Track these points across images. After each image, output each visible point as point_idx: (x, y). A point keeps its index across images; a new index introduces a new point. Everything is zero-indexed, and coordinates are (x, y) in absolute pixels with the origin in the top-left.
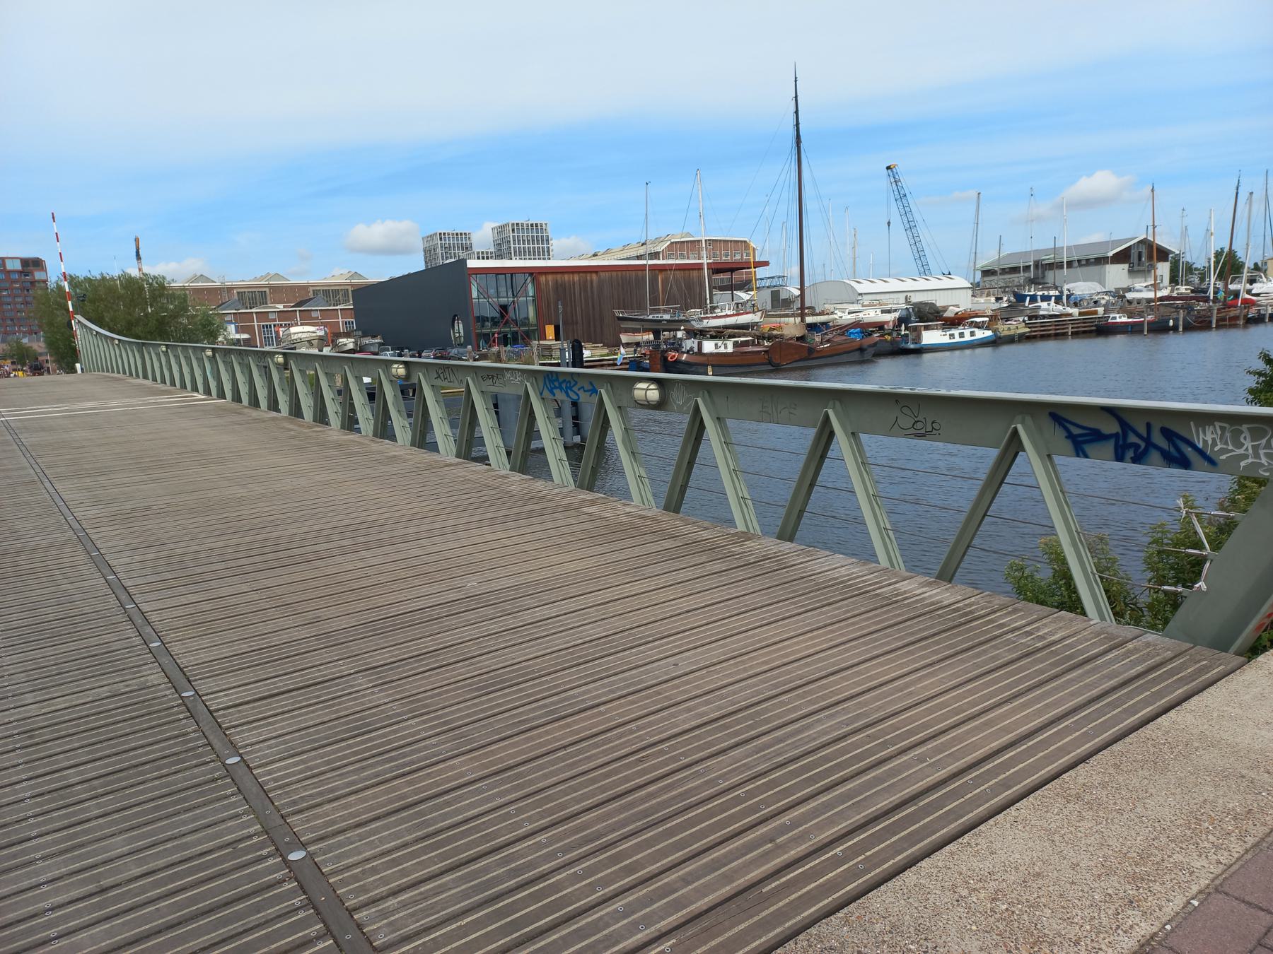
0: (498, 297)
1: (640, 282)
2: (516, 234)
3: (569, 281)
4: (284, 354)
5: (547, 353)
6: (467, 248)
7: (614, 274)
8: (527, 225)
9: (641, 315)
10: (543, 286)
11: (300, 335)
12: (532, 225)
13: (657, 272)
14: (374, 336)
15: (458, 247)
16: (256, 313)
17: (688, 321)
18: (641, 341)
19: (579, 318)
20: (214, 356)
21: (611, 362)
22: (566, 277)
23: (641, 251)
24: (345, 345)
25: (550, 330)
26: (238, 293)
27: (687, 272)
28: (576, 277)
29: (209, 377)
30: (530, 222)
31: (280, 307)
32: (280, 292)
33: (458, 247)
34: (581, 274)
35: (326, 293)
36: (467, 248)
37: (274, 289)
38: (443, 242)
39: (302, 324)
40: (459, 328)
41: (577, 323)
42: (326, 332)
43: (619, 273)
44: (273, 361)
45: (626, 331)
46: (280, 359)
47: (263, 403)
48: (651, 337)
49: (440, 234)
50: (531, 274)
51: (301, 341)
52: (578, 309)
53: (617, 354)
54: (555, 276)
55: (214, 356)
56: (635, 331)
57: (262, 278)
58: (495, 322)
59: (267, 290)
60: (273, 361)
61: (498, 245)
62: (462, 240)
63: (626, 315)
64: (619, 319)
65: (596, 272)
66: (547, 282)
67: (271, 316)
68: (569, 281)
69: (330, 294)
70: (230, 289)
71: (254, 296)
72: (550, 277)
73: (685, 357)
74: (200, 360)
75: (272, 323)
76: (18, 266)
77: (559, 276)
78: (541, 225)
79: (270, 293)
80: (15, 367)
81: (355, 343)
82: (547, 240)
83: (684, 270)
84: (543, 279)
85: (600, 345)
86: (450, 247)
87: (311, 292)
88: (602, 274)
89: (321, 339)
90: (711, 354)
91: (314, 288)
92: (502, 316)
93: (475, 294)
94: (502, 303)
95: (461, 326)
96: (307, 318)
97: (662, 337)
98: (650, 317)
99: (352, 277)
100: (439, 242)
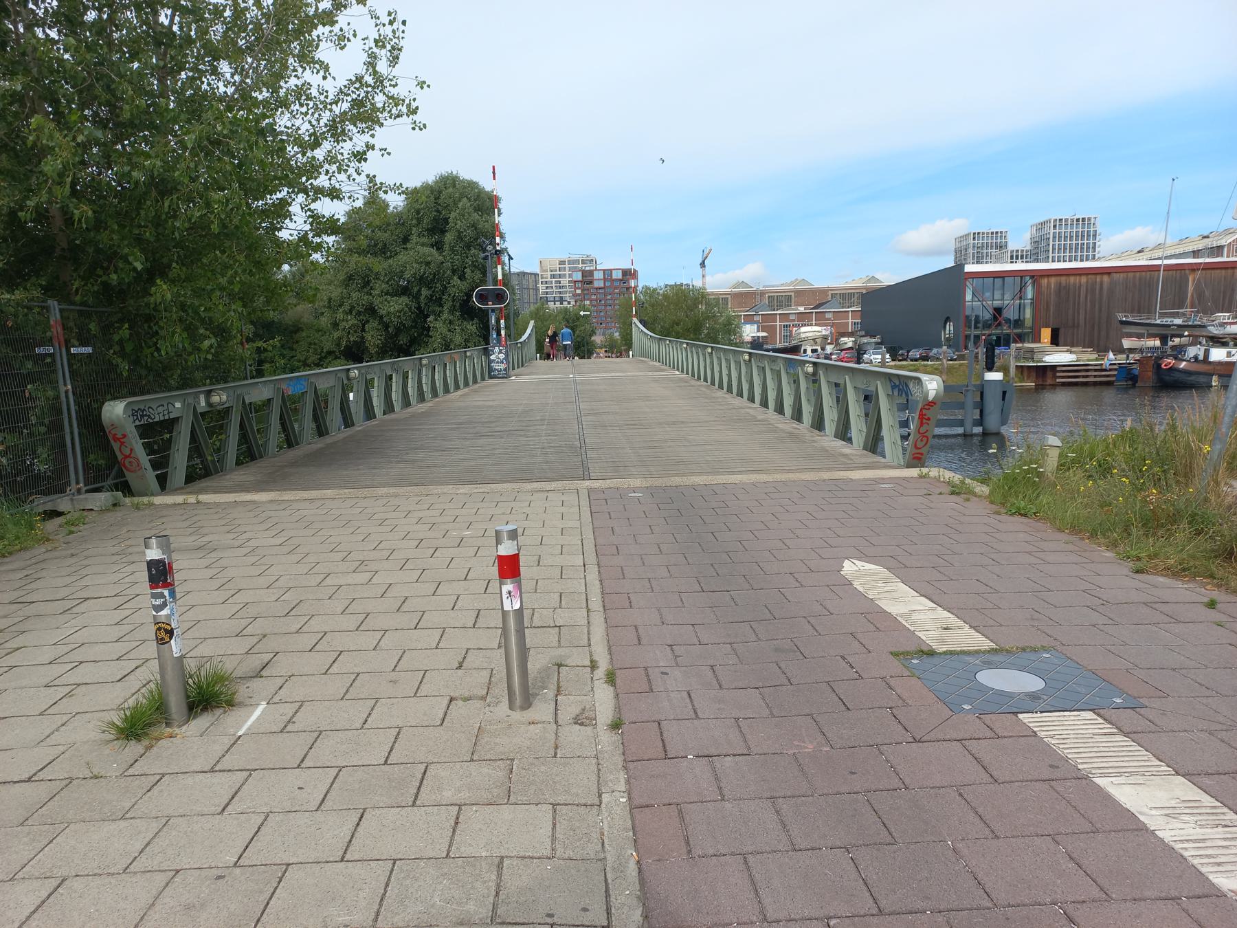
0: (993, 300)
1: (1150, 286)
2: (1057, 231)
3: (1075, 284)
4: (815, 364)
5: (1029, 355)
6: (1001, 247)
7: (1131, 275)
8: (1072, 220)
9: (1149, 319)
10: (1044, 289)
11: (807, 334)
12: (992, 233)
13: (1187, 272)
14: (872, 336)
15: (992, 247)
16: (780, 314)
17: (1204, 327)
18: (1144, 347)
19: (1082, 322)
20: (750, 360)
21: (1099, 368)
22: (1072, 279)
23: (1200, 245)
24: (846, 343)
25: (1046, 334)
26: (769, 297)
27: (1230, 271)
28: (1084, 279)
29: (743, 377)
30: (1075, 217)
31: (801, 309)
32: (803, 295)
33: (992, 247)
34: (1090, 276)
35: (843, 296)
36: (1001, 247)
37: (799, 293)
38: (976, 242)
39: (816, 325)
40: (950, 328)
41: (1078, 326)
42: (831, 333)
43: (1138, 274)
44: (803, 370)
45: (1130, 336)
46: (810, 369)
47: (788, 410)
48: (1158, 343)
49: (974, 234)
50: (1032, 277)
51: (807, 339)
52: (1082, 312)
53: (1103, 360)
54: (1058, 278)
55: (750, 360)
56: (1139, 336)
57: (791, 283)
58: (987, 325)
59: (793, 294)
60: (803, 370)
61: (1036, 243)
62: (1083, 228)
63: (1130, 319)
64: (1122, 322)
65: (1109, 273)
66: (1049, 284)
67: (792, 317)
68: (1075, 284)
69: (844, 296)
70: (763, 293)
71: (781, 300)
72: (1053, 280)
73: (1183, 365)
74: (738, 363)
75: (791, 324)
76: (620, 276)
77: (1063, 279)
78: (1089, 219)
79: (795, 297)
80: (607, 355)
81: (855, 342)
82: (1095, 236)
83: (1226, 268)
84: (1044, 281)
85: (1089, 350)
86: (983, 246)
87: (830, 296)
88: (1116, 276)
89: (825, 338)
90: (1220, 363)
91: (833, 292)
92: (995, 318)
93: (969, 297)
94: (995, 306)
95: (952, 328)
96: (821, 319)
97: (1170, 343)
98: (1158, 322)
99: (869, 281)
100: (972, 242)
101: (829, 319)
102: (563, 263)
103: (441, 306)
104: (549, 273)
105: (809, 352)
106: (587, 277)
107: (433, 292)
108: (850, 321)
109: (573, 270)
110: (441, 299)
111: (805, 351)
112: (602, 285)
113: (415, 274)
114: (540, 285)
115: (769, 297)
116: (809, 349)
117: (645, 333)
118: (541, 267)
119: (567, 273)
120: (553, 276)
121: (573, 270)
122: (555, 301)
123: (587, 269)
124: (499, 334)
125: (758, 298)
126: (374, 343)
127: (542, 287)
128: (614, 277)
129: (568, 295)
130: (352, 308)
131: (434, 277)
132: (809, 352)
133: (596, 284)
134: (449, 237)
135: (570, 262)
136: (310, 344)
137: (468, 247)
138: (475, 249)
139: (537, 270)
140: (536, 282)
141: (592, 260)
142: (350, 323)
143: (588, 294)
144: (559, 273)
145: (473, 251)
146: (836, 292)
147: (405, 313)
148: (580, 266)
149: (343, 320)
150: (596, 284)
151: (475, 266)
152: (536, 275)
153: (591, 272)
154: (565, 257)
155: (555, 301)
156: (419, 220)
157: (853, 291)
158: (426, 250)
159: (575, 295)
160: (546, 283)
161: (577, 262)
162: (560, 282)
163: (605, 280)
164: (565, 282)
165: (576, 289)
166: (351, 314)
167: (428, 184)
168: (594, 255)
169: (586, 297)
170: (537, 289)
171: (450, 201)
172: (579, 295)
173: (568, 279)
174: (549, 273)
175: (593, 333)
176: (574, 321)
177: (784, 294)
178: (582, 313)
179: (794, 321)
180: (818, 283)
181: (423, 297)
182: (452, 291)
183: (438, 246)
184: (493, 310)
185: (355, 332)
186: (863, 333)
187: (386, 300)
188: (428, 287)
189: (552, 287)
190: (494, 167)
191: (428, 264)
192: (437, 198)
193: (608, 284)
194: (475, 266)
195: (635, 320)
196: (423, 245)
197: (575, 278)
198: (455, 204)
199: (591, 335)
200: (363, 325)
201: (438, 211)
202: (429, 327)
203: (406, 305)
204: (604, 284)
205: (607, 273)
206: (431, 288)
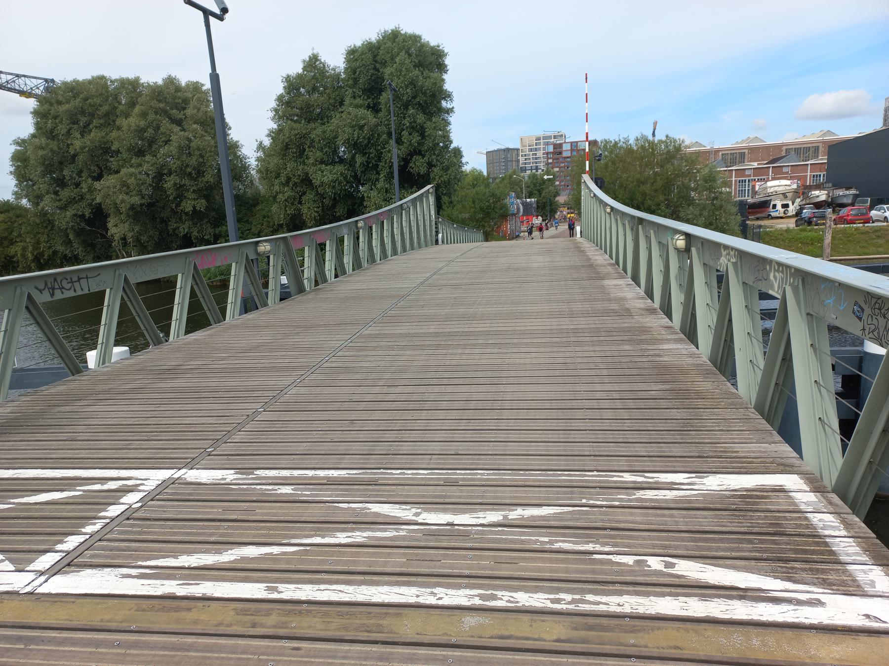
11: (776, 189)
14: (848, 188)
16: (736, 170)
24: (818, 197)
31: (755, 165)
32: (755, 152)
37: (753, 150)
51: (776, 194)
57: (743, 142)
59: (746, 151)
67: (747, 173)
69: (803, 151)
70: (717, 151)
75: (747, 179)
79: (749, 153)
81: (828, 195)
87: (784, 151)
101: (787, 173)
102: (538, 139)
103: (378, 173)
104: (528, 148)
105: (779, 207)
106: (558, 148)
107: (368, 158)
108: (809, 174)
110: (377, 166)
111: (774, 206)
112: (569, 155)
113: (348, 139)
114: (520, 158)
115: (723, 154)
116: (779, 204)
117: (601, 202)
119: (542, 146)
120: (531, 150)
121: (547, 144)
122: (531, 170)
123: (558, 142)
125: (712, 156)
126: (311, 216)
127: (522, 159)
129: (542, 164)
130: (289, 179)
131: (369, 142)
132: (779, 207)
133: (565, 154)
134: (386, 97)
135: (544, 138)
136: (264, 217)
137: (406, 106)
138: (413, 108)
139: (517, 145)
140: (518, 155)
141: (562, 135)
142: (286, 195)
143: (558, 162)
144: (535, 147)
145: (411, 111)
146: (791, 147)
147: (340, 183)
148: (552, 140)
149: (280, 192)
150: (565, 154)
151: (413, 128)
152: (518, 150)
153: (561, 145)
154: (540, 134)
155: (531, 170)
156: (356, 81)
157: (809, 145)
158: (362, 112)
159: (548, 164)
160: (525, 155)
161: (550, 137)
162: (536, 154)
163: (572, 150)
164: (540, 154)
165: (548, 159)
166: (288, 186)
167: (370, 43)
168: (564, 131)
169: (556, 165)
170: (518, 161)
171: (387, 58)
172: (551, 163)
173: (542, 152)
174: (528, 148)
175: (557, 194)
176: (540, 185)
177: (729, 152)
178: (546, 177)
179: (750, 176)
180: (771, 140)
181: (357, 165)
183: (375, 108)
185: (293, 204)
186: (830, 185)
187: (320, 169)
188: (363, 153)
189: (530, 159)
191: (361, 128)
192: (375, 56)
193: (575, 153)
194: (413, 128)
195: (586, 178)
196: (357, 106)
198: (392, 59)
199: (555, 196)
200: (300, 198)
201: (375, 69)
202: (363, 197)
203: (342, 174)
204: (571, 153)
205: (574, 145)
206: (366, 153)
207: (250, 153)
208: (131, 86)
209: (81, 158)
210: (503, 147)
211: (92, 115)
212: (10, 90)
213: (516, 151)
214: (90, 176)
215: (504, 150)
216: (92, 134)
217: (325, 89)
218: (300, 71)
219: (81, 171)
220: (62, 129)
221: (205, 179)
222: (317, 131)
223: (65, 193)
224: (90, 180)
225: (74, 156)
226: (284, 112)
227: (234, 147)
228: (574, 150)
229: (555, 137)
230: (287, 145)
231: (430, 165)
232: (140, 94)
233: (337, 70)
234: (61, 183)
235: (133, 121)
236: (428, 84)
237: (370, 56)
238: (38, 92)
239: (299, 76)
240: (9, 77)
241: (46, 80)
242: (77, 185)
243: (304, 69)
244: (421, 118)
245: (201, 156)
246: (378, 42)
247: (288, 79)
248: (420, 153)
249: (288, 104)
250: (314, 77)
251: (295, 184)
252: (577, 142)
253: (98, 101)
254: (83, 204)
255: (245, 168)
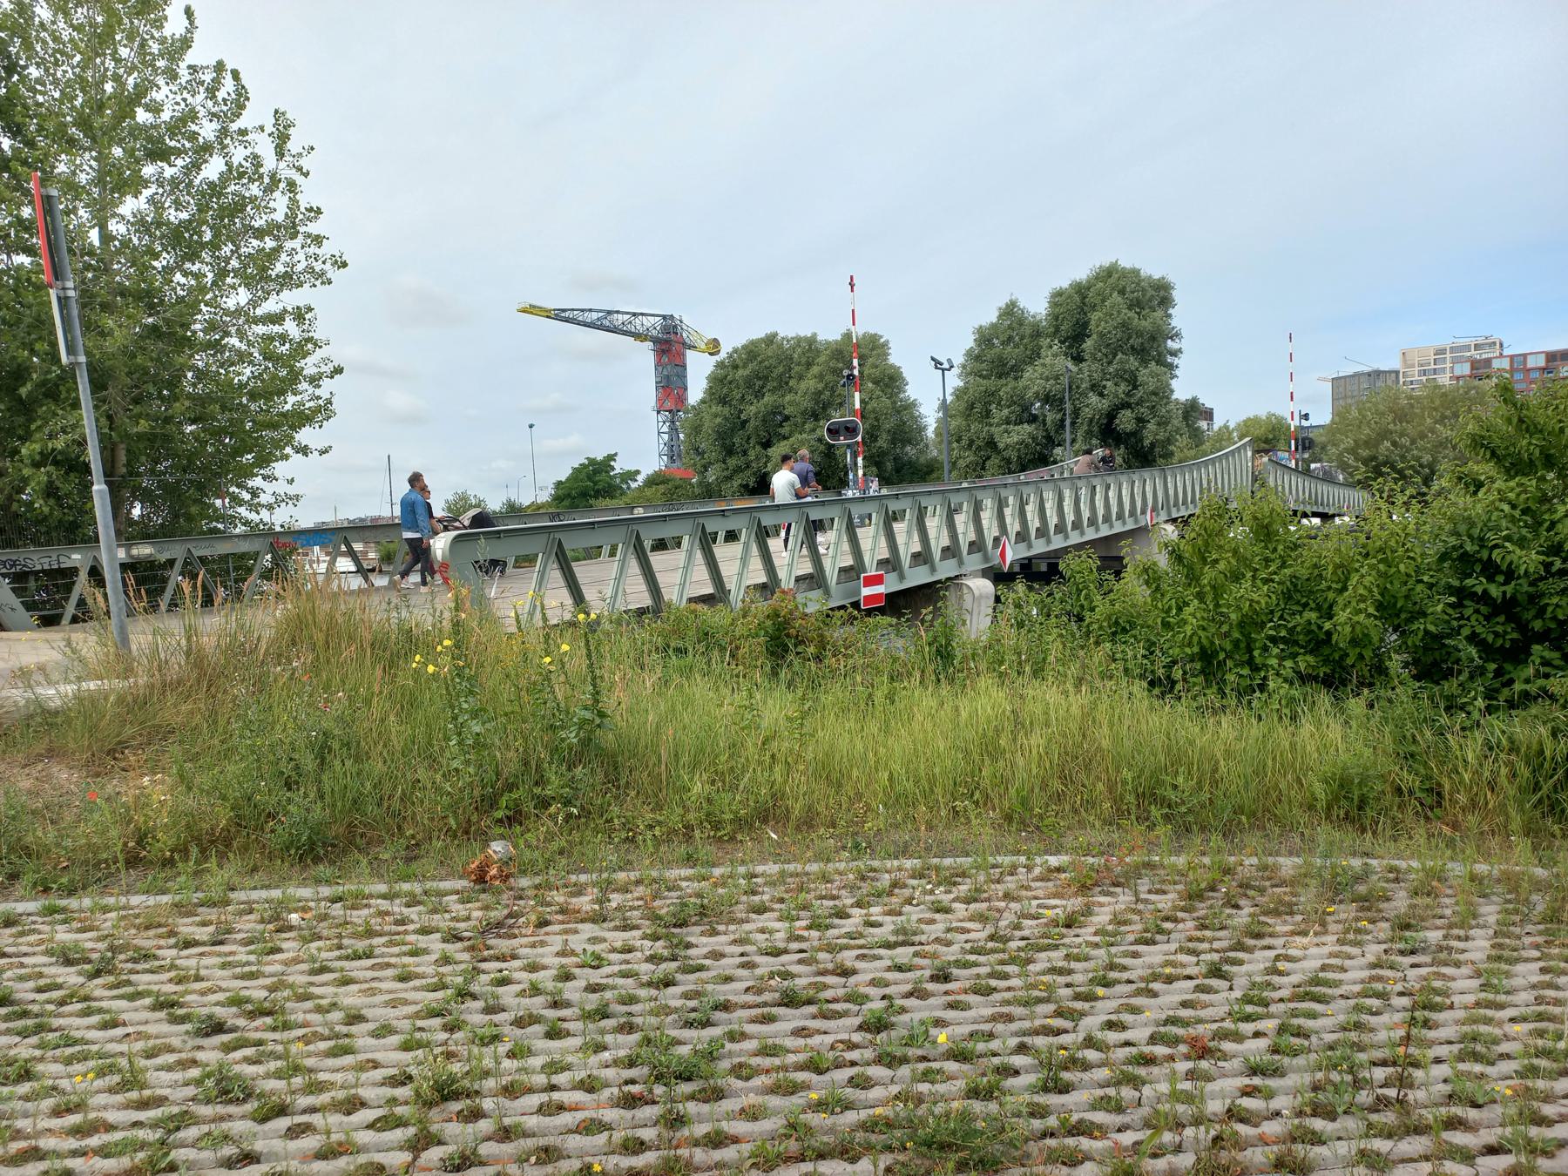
102: (1441, 351)
104: (1417, 369)
109: (1455, 361)
118: (1405, 361)
123: (1484, 356)
124: (856, 475)
128: (1531, 363)
130: (971, 442)
135: (1453, 350)
141: (1494, 343)
142: (968, 460)
144: (1433, 367)
152: (1397, 373)
153: (1488, 361)
154: (1446, 342)
156: (1057, 330)
161: (1468, 348)
171: (1097, 300)
173: (1448, 375)
182: (1087, 412)
183: (1078, 359)
184: (848, 446)
185: (974, 470)
190: (531, 310)
191: (1057, 378)
197: (1458, 373)
200: (984, 463)
205: (1519, 361)
207: (930, 417)
208: (809, 347)
209: (752, 424)
210: (1366, 369)
211: (766, 378)
212: (625, 333)
213: (1393, 375)
214: (758, 443)
215: (1369, 374)
216: (766, 399)
217: (1021, 339)
218: (994, 320)
219: (749, 438)
220: (737, 395)
221: (878, 444)
222: (1006, 388)
223: (733, 462)
224: (758, 448)
225: (746, 422)
226: (972, 369)
227: (911, 406)
228: (1518, 370)
229: (1477, 347)
230: (973, 404)
231: (1140, 420)
232: (818, 352)
233: (1038, 318)
234: (730, 452)
235: (810, 384)
236: (1146, 324)
237: (1077, 298)
238: (654, 333)
239: (993, 326)
240: (601, 314)
241: (664, 317)
242: (745, 453)
243: (1000, 317)
244: (1133, 362)
245: (877, 419)
246: (1088, 281)
247: (980, 330)
248: (1126, 406)
249: (978, 358)
250: (1010, 327)
251: (979, 448)
252: (1525, 356)
253: (773, 362)
254: (748, 473)
255: (922, 429)
